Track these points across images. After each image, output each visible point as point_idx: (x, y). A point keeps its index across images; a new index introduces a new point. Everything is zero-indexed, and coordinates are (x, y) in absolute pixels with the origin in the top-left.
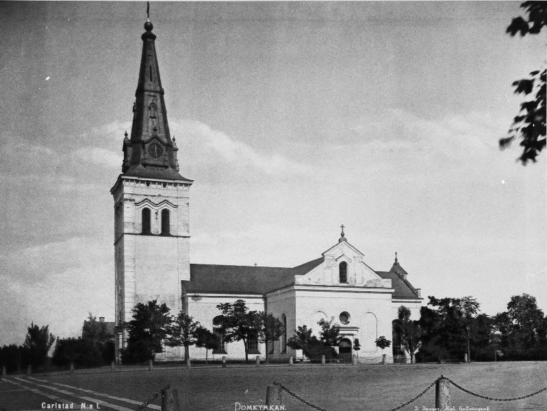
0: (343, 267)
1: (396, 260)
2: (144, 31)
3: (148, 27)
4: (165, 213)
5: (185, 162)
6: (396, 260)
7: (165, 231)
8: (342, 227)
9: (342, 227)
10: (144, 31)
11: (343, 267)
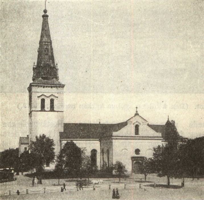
0: (137, 127)
1: (168, 119)
2: (43, 13)
3: (45, 11)
4: (52, 101)
5: (63, 76)
6: (168, 119)
7: (52, 109)
8: (137, 108)
9: (137, 108)
10: (43, 13)
11: (137, 127)
